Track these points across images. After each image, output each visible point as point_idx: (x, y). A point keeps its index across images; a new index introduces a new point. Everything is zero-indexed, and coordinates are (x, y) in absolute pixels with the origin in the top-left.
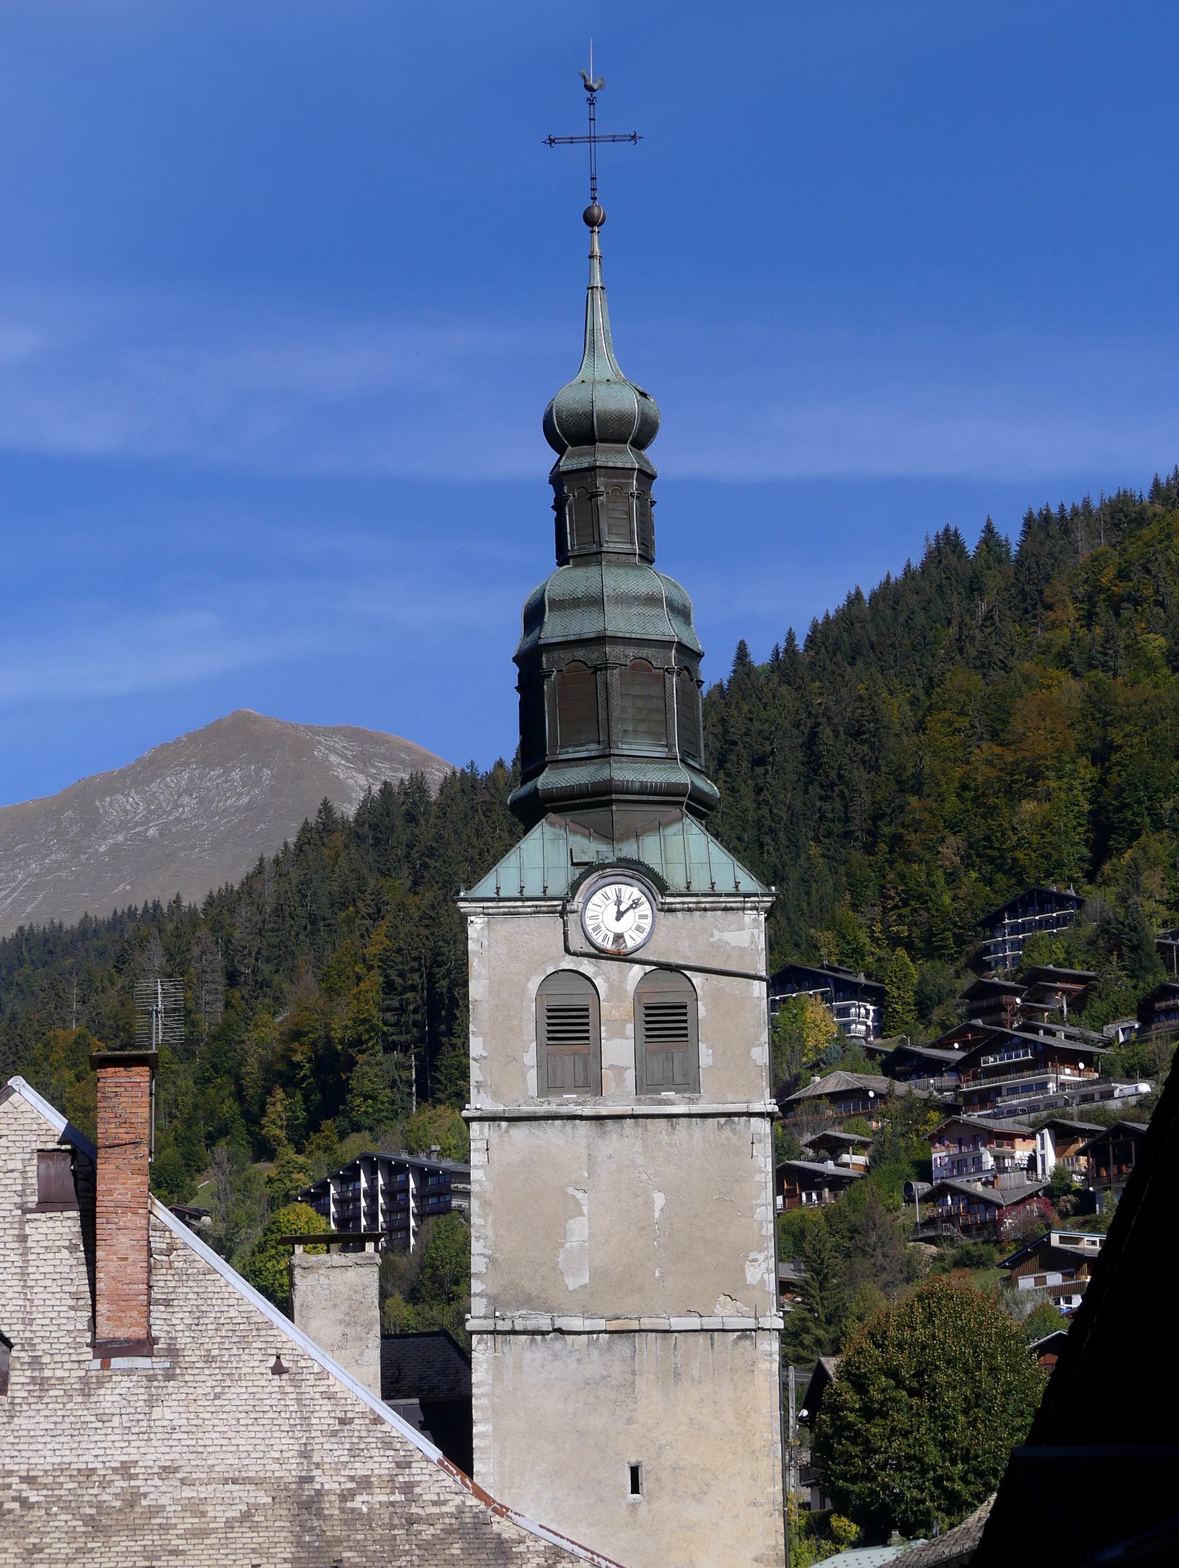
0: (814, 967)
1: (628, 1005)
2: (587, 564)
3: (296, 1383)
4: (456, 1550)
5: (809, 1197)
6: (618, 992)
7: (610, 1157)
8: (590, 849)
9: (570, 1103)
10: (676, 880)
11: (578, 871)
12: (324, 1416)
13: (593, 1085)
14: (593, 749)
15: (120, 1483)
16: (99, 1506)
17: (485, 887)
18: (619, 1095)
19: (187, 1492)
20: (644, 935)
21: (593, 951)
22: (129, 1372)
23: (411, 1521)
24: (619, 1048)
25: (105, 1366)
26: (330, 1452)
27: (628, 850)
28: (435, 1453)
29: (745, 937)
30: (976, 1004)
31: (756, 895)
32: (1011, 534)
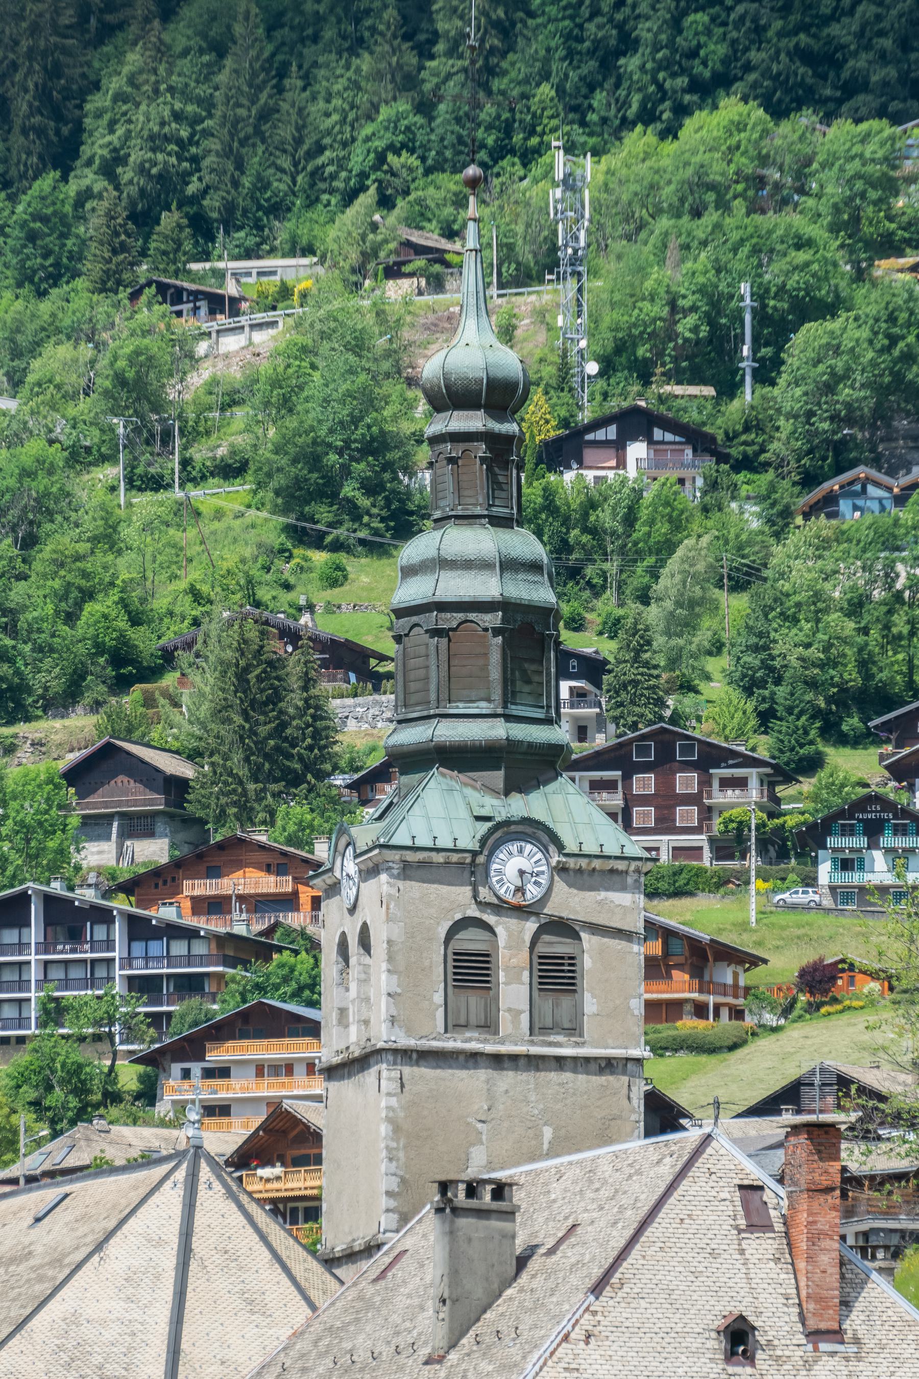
6: (512, 942)
7: (507, 1092)
13: (489, 1026)
14: (484, 707)
20: (543, 890)
21: (495, 901)
24: (513, 991)
31: (640, 859)
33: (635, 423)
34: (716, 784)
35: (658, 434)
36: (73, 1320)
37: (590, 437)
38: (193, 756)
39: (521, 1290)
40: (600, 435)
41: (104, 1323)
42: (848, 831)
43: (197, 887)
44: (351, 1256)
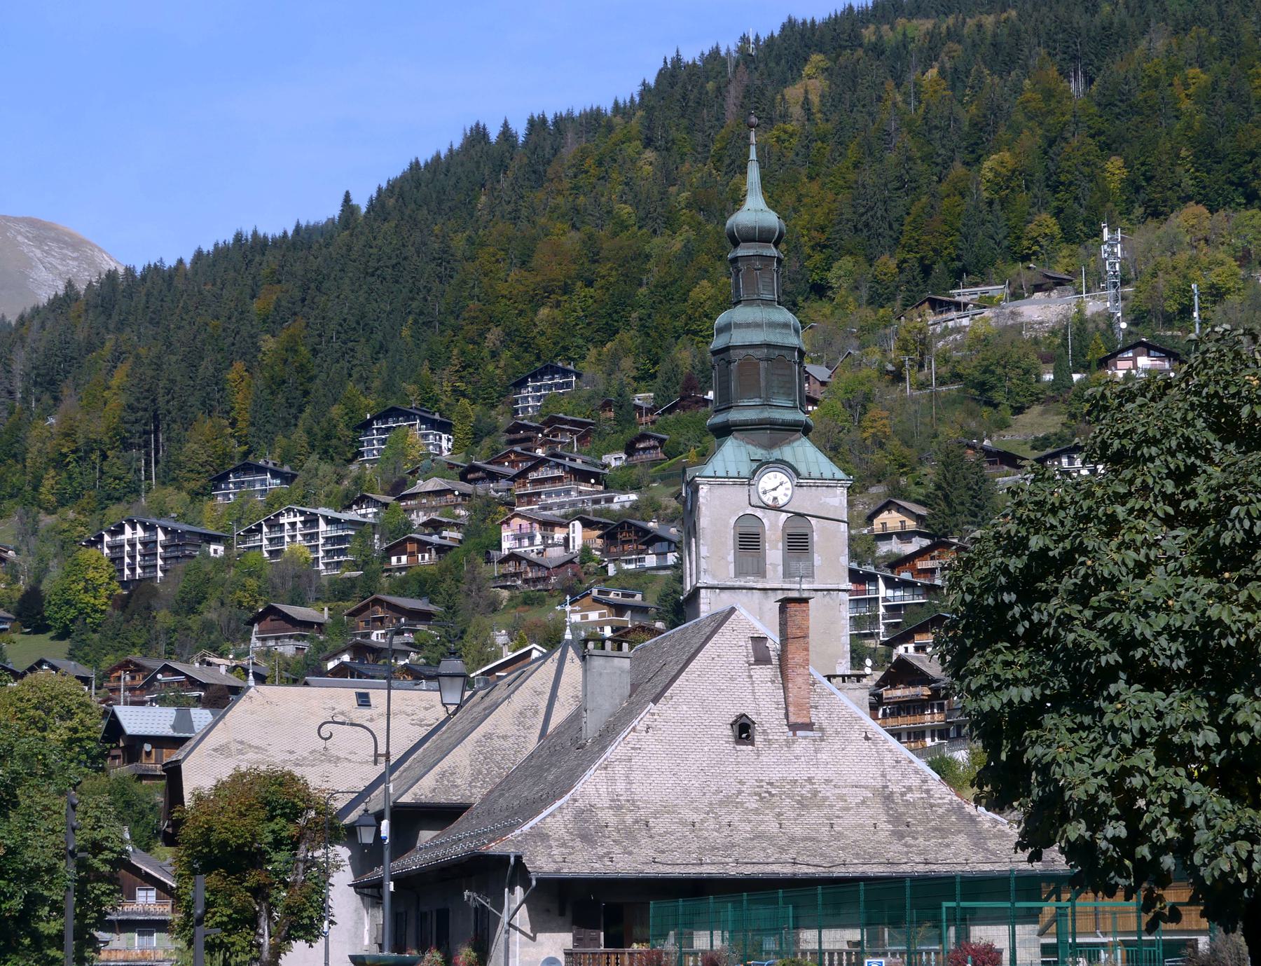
0: (407, 408)
1: (780, 533)
2: (751, 305)
3: (875, 744)
4: (953, 819)
5: (423, 558)
6: (773, 527)
8: (759, 453)
9: (750, 581)
10: (803, 470)
11: (755, 465)
12: (889, 760)
13: (761, 573)
14: (757, 401)
16: (802, 796)
17: (708, 470)
19: (837, 791)
22: (805, 738)
23: (932, 806)
24: (774, 553)
25: (795, 735)
26: (893, 775)
27: (776, 454)
28: (937, 777)
29: (837, 500)
30: (512, 436)
32: (520, 129)
36: (489, 736)
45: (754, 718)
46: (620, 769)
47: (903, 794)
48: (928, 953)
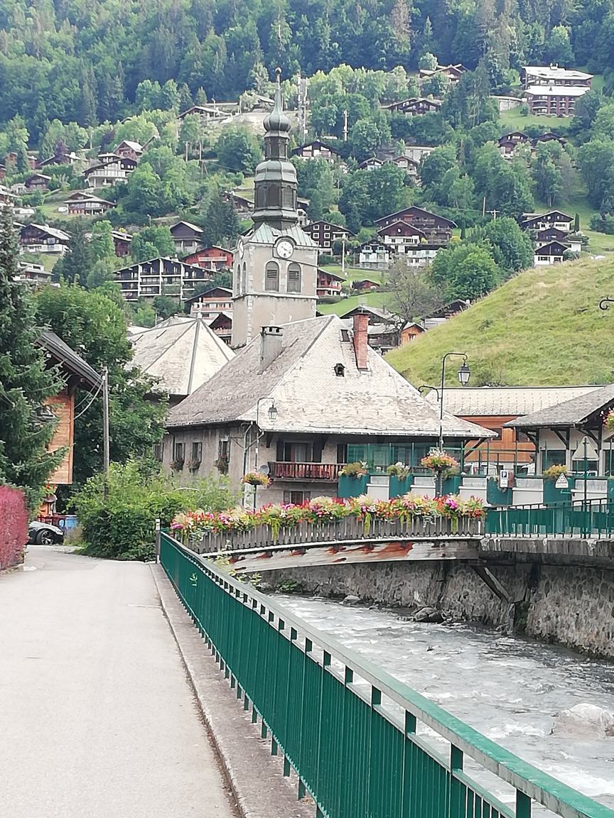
6: (284, 268)
8: (277, 232)
12: (399, 386)
14: (277, 207)
15: (367, 396)
18: (283, 291)
24: (283, 281)
27: (284, 233)
33: (317, 146)
34: (334, 236)
35: (322, 148)
36: (166, 362)
37: (304, 149)
38: (201, 227)
39: (283, 356)
40: (307, 148)
41: (174, 363)
42: (368, 249)
43: (201, 259)
44: (238, 347)
45: (344, 365)
46: (290, 386)
47: (405, 400)
48: (298, 465)
